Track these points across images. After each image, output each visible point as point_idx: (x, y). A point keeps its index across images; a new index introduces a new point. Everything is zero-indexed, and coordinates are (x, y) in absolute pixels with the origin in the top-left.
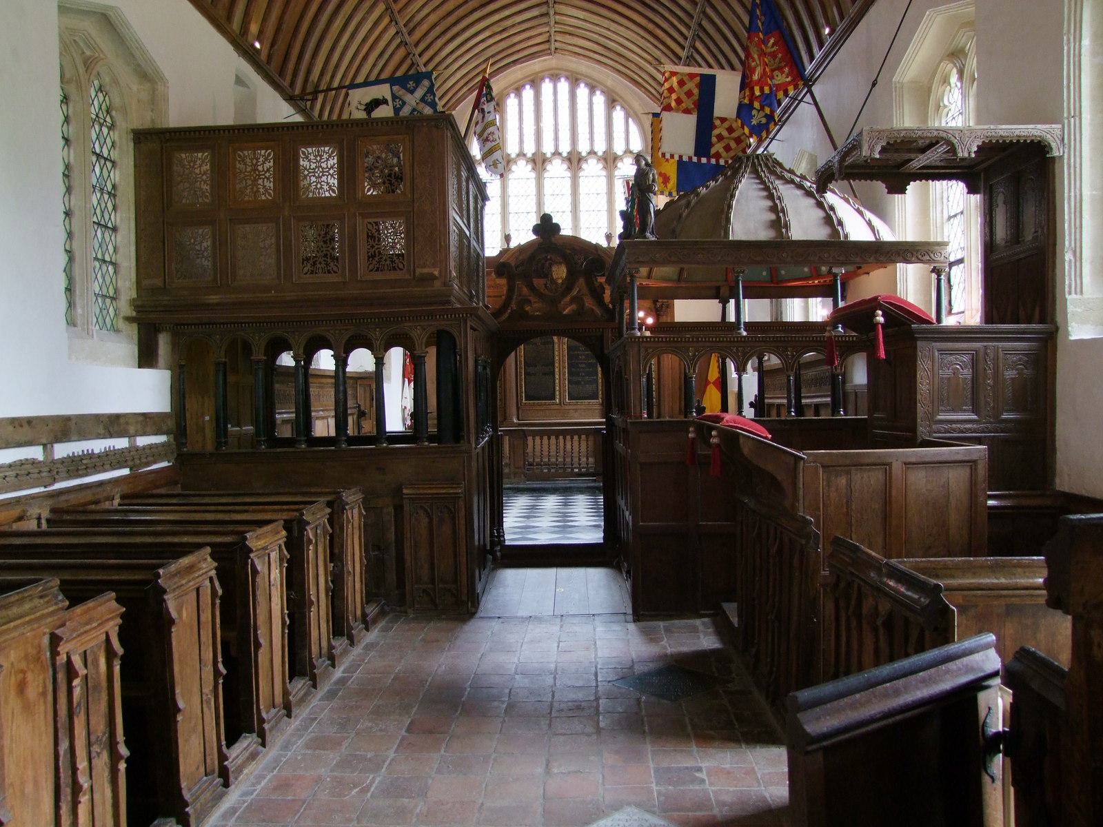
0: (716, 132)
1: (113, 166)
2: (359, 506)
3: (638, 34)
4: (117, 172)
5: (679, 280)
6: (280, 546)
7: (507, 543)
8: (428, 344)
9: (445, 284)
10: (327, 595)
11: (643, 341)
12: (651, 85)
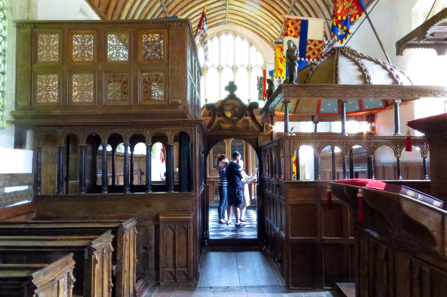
0: (308, 46)
1: (4, 39)
2: (134, 229)
3: (264, 13)
4: (6, 42)
5: (295, 112)
6: (68, 273)
7: (211, 238)
8: (175, 141)
9: (184, 108)
10: (109, 291)
11: (292, 138)
12: (268, 37)
